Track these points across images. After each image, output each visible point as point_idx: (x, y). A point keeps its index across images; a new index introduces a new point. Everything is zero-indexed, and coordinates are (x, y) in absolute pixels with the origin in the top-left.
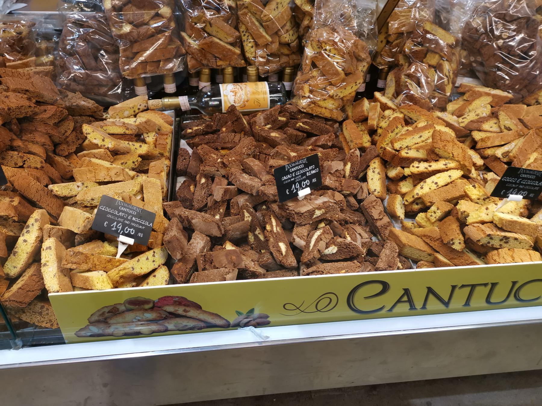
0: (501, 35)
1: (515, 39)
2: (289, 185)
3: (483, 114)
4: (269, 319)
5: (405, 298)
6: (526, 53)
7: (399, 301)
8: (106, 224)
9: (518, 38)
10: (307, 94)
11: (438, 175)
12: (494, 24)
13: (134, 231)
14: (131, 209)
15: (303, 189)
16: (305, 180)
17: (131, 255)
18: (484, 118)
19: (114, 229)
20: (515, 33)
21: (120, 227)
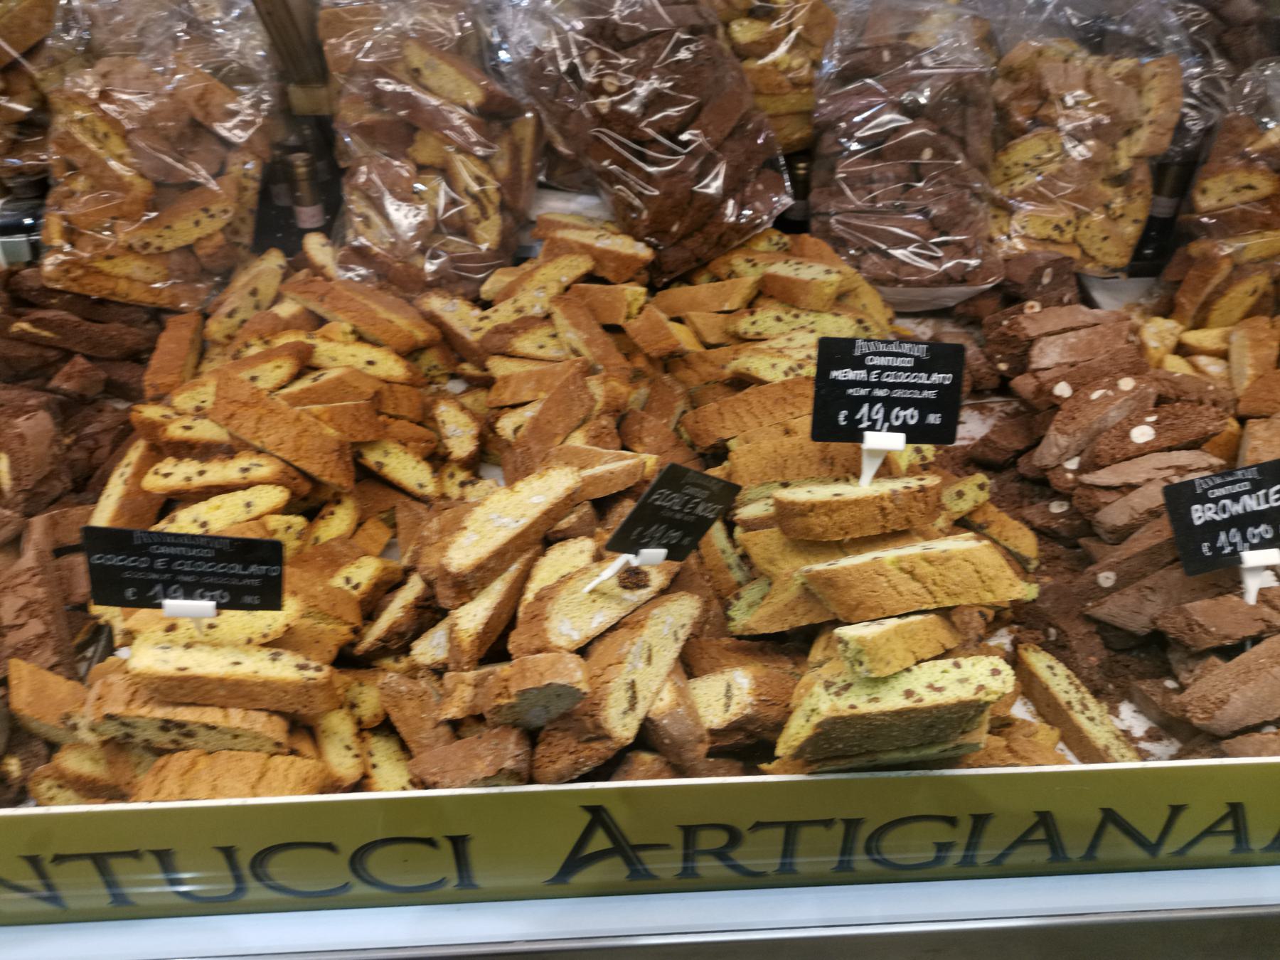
0: (599, 85)
1: (634, 94)
3: (533, 306)
5: (1040, 834)
6: (673, 137)
7: (1210, 831)
9: (642, 90)
10: (57, 242)
11: (215, 500)
12: (574, 51)
15: (1253, 547)
18: (533, 318)
20: (631, 79)
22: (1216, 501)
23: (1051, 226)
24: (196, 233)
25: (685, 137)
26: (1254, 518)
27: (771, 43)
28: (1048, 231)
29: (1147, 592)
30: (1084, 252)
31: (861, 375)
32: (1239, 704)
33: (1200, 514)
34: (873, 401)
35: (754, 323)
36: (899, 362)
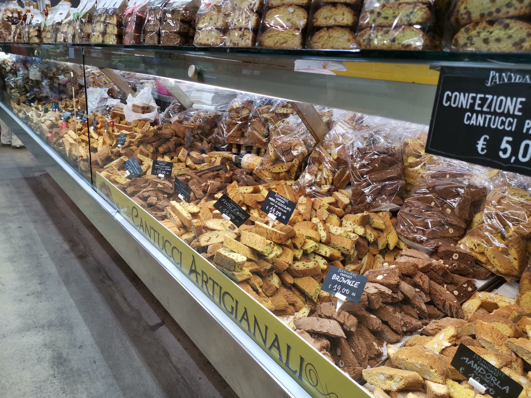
2: (157, 169)
6: (362, 176)
14: (348, 275)
15: (341, 293)
16: (164, 171)
17: (316, 336)
19: (335, 290)
21: (339, 289)
24: (279, 171)
27: (417, 164)
31: (274, 200)
32: (302, 321)
34: (274, 207)
36: (282, 201)
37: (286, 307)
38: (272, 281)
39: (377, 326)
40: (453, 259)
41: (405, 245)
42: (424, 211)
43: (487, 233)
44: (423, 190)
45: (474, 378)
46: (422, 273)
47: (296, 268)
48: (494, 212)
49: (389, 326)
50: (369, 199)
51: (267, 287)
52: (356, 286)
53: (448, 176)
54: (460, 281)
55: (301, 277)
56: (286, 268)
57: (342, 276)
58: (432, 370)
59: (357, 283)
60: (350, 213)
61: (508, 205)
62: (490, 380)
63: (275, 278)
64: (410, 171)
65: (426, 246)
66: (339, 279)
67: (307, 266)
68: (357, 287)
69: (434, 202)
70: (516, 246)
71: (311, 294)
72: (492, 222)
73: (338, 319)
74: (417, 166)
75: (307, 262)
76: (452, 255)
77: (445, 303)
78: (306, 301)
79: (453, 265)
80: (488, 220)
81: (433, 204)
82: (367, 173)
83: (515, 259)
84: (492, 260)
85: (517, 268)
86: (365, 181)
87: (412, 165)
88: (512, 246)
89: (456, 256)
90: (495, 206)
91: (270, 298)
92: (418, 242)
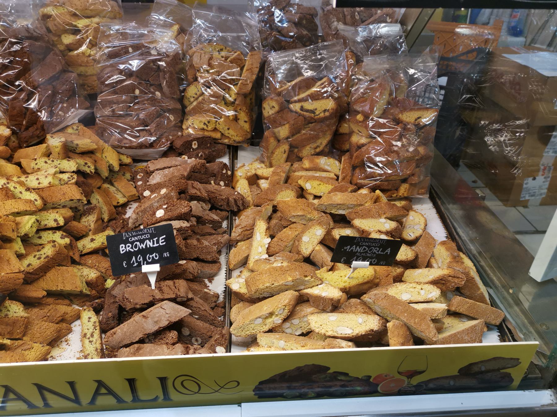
4: (254, 393)
6: (12, 83)
8: (125, 264)
13: (157, 254)
14: (141, 235)
15: (148, 263)
19: (135, 265)
21: (141, 259)
22: (132, 243)
23: (203, 123)
25: (17, 83)
26: (151, 250)
27: (79, 44)
28: (202, 126)
29: (128, 283)
30: (222, 134)
32: (120, 334)
33: (123, 249)
35: (36, 164)
37: (60, 331)
38: (11, 314)
39: (196, 271)
40: (193, 149)
41: (127, 157)
42: (132, 105)
43: (212, 106)
44: (115, 77)
45: (356, 260)
46: (191, 182)
47: (28, 268)
48: (210, 78)
49: (203, 261)
50: (43, 116)
51: (9, 329)
52: (162, 242)
53: (130, 50)
54: (215, 169)
55: (42, 276)
56: (22, 281)
57: (134, 242)
58: (307, 279)
59: (161, 238)
60: (20, 147)
61: (220, 65)
62: (372, 253)
63: (12, 306)
64: (73, 56)
65: (160, 147)
66: (132, 248)
67: (44, 256)
68: (164, 243)
69: (138, 88)
70: (244, 108)
71: (79, 290)
72: (212, 90)
73: (166, 298)
74: (81, 46)
75: (39, 251)
76: (191, 145)
77: (228, 200)
78: (71, 300)
79: (200, 155)
80: (208, 90)
81: (137, 92)
82: (18, 77)
83: (245, 122)
84: (226, 133)
85: (248, 130)
86: (22, 90)
87: (71, 48)
88: (240, 109)
89: (195, 144)
90: (208, 71)
91: (24, 338)
92: (146, 147)
